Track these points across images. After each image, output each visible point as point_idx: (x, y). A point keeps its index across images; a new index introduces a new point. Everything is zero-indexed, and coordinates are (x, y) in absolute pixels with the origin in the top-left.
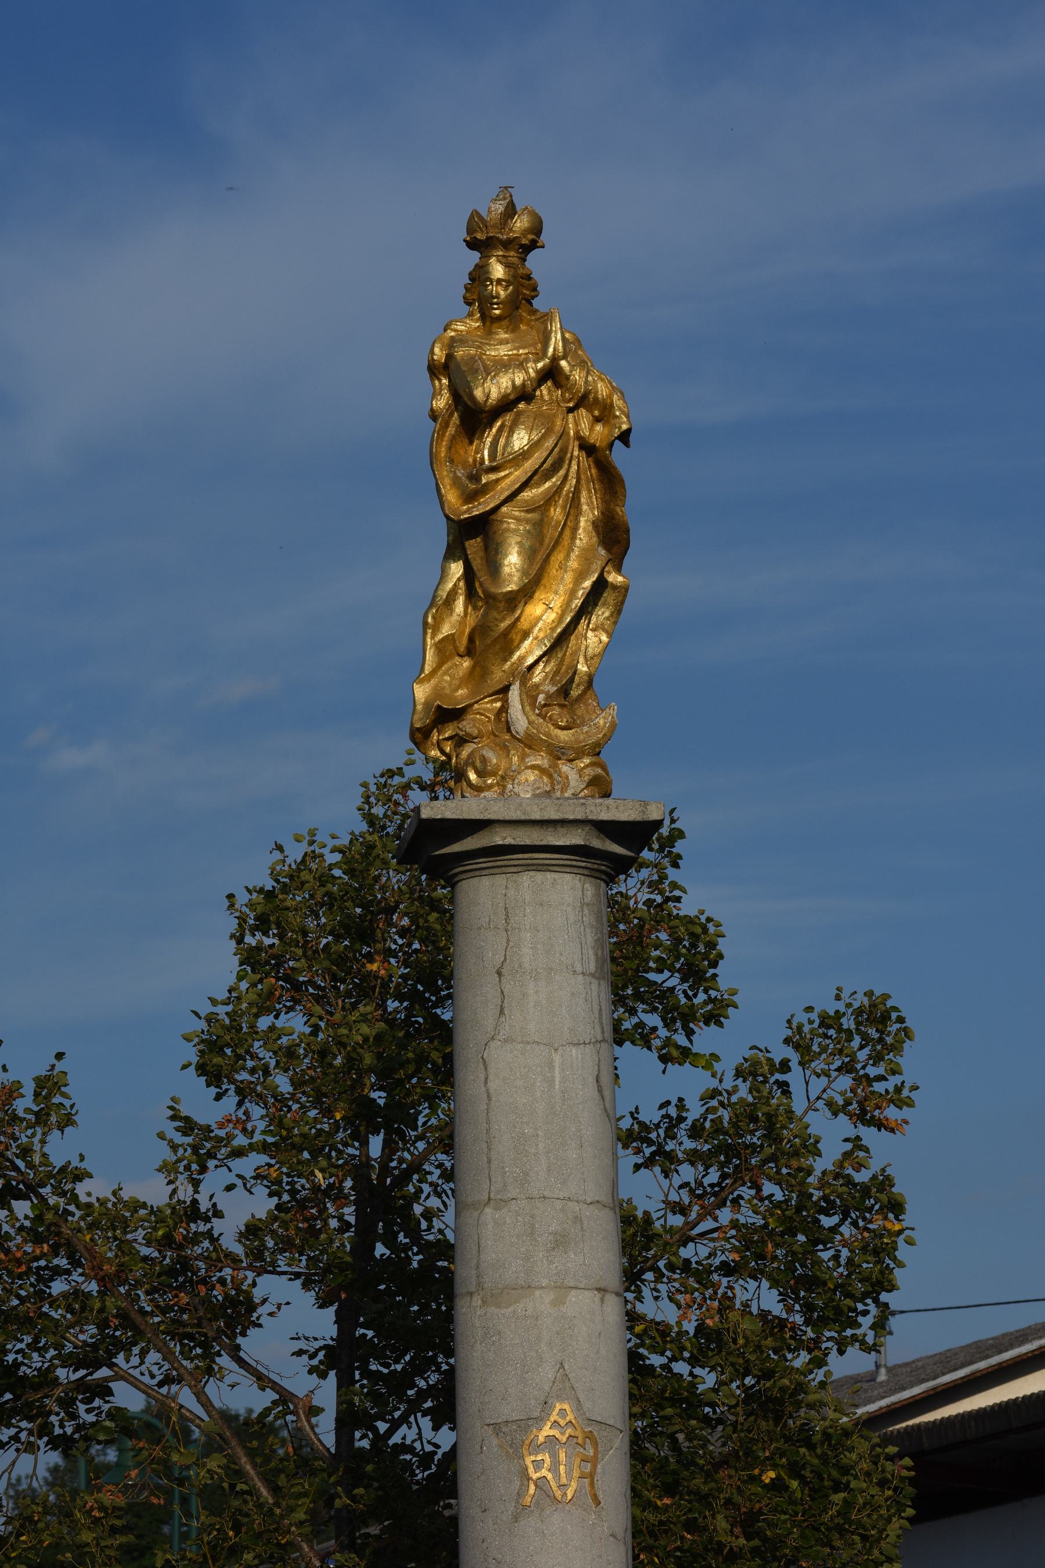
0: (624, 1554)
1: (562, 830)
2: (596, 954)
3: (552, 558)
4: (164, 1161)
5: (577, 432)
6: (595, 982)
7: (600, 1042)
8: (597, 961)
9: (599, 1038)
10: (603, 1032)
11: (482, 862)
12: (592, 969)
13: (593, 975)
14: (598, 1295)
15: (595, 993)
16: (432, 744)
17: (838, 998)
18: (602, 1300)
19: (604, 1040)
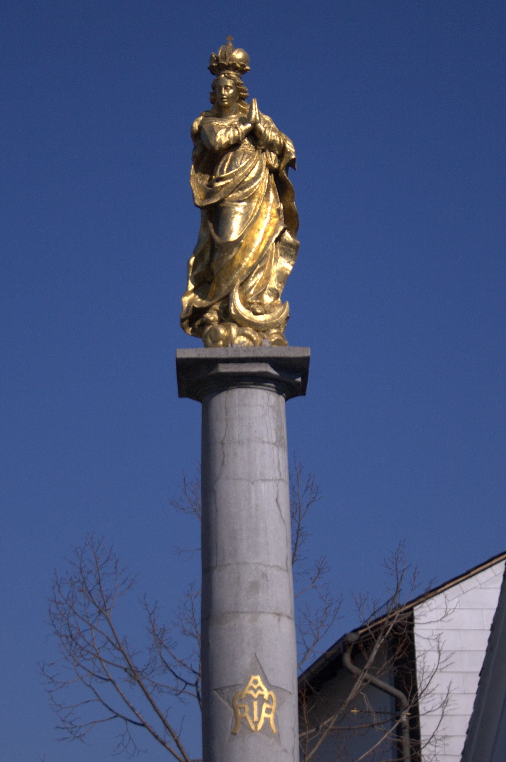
0: (263, 391)
1: (254, 364)
2: (277, 433)
3: (264, 364)
4: (209, 68)
5: (267, 163)
6: (275, 449)
7: (279, 480)
8: (277, 437)
9: (278, 478)
10: (280, 475)
11: (126, 661)
12: (274, 440)
13: (274, 444)
14: (276, 618)
15: (276, 454)
16: (198, 120)
17: (392, 575)
18: (279, 620)
19: (281, 479)
